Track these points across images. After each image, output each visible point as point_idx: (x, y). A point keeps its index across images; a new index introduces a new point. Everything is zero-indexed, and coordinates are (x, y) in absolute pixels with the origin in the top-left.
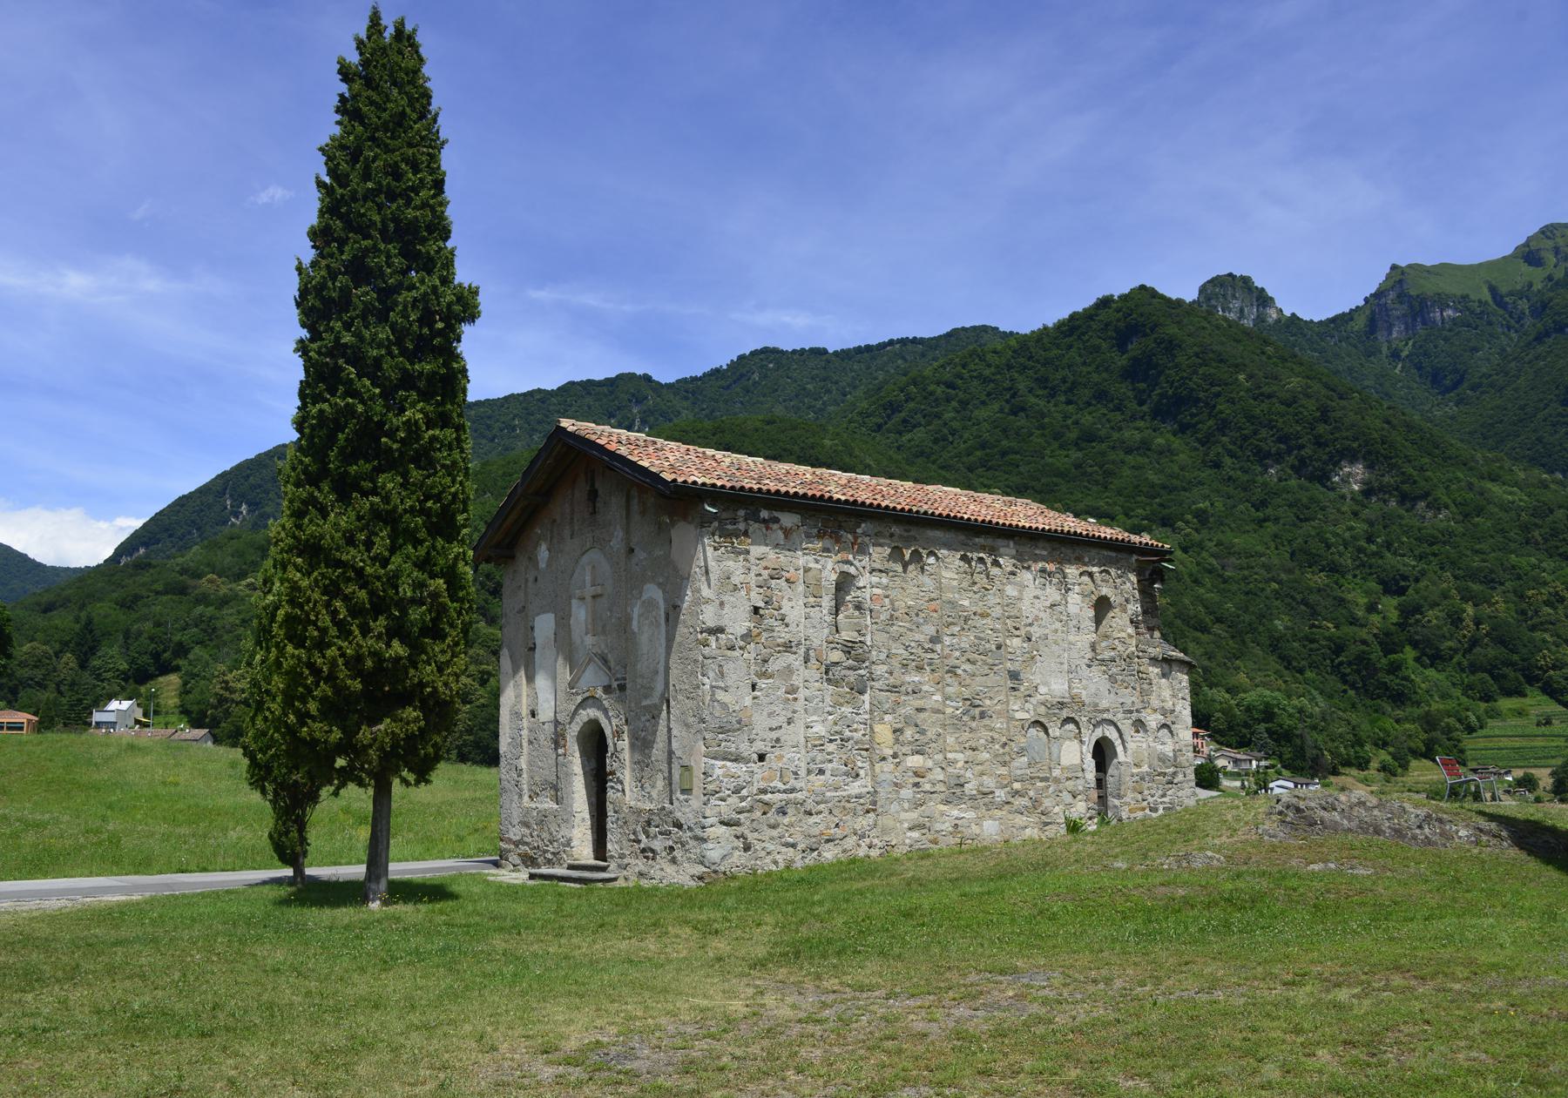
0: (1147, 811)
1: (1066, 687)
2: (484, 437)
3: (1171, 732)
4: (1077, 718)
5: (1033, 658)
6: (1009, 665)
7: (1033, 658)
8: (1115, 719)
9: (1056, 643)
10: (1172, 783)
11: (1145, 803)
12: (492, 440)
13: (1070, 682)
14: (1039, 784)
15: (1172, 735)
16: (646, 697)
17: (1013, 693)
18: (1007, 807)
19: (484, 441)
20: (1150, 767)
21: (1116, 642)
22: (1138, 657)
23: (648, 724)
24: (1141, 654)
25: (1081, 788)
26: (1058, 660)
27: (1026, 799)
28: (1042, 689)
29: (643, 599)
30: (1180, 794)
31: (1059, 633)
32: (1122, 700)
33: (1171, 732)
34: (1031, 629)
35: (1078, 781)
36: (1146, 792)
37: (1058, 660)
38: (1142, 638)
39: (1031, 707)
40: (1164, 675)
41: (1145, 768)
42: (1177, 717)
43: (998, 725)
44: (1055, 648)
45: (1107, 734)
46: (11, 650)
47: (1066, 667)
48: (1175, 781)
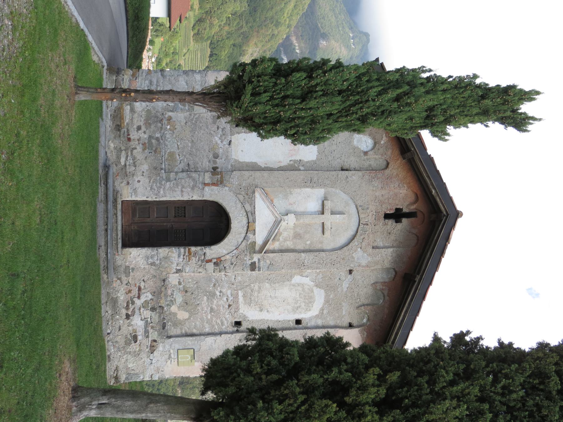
16: (244, 296)
23: (225, 299)
29: (315, 288)
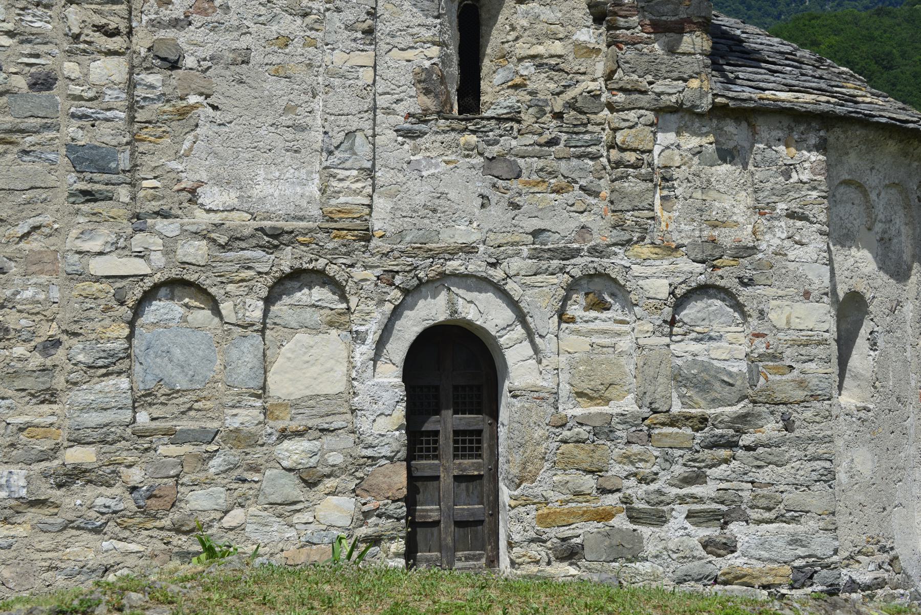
0: (620, 522)
1: (313, 189)
2: (769, 15)
3: (739, 307)
4: (332, 270)
5: (183, 114)
6: (72, 130)
7: (183, 114)
8: (497, 274)
9: (281, 73)
10: (731, 445)
11: (611, 500)
12: (778, 17)
13: (328, 173)
14: (167, 450)
15: (745, 315)
17: (85, 208)
18: (33, 514)
19: (769, 20)
20: (639, 400)
21: (527, 69)
22: (611, 107)
24: (620, 97)
25: (336, 459)
26: (286, 120)
27: (117, 490)
28: (211, 197)
30: (763, 476)
31: (296, 47)
32: (537, 224)
33: (739, 307)
34: (182, 38)
35: (328, 439)
36: (617, 469)
37: (286, 120)
38: (629, 54)
39: (155, 243)
40: (726, 155)
41: (627, 404)
42: (758, 267)
43: (28, 294)
44: (274, 86)
45: (469, 313)
46: (128, 325)
47: (316, 137)
48: (746, 440)
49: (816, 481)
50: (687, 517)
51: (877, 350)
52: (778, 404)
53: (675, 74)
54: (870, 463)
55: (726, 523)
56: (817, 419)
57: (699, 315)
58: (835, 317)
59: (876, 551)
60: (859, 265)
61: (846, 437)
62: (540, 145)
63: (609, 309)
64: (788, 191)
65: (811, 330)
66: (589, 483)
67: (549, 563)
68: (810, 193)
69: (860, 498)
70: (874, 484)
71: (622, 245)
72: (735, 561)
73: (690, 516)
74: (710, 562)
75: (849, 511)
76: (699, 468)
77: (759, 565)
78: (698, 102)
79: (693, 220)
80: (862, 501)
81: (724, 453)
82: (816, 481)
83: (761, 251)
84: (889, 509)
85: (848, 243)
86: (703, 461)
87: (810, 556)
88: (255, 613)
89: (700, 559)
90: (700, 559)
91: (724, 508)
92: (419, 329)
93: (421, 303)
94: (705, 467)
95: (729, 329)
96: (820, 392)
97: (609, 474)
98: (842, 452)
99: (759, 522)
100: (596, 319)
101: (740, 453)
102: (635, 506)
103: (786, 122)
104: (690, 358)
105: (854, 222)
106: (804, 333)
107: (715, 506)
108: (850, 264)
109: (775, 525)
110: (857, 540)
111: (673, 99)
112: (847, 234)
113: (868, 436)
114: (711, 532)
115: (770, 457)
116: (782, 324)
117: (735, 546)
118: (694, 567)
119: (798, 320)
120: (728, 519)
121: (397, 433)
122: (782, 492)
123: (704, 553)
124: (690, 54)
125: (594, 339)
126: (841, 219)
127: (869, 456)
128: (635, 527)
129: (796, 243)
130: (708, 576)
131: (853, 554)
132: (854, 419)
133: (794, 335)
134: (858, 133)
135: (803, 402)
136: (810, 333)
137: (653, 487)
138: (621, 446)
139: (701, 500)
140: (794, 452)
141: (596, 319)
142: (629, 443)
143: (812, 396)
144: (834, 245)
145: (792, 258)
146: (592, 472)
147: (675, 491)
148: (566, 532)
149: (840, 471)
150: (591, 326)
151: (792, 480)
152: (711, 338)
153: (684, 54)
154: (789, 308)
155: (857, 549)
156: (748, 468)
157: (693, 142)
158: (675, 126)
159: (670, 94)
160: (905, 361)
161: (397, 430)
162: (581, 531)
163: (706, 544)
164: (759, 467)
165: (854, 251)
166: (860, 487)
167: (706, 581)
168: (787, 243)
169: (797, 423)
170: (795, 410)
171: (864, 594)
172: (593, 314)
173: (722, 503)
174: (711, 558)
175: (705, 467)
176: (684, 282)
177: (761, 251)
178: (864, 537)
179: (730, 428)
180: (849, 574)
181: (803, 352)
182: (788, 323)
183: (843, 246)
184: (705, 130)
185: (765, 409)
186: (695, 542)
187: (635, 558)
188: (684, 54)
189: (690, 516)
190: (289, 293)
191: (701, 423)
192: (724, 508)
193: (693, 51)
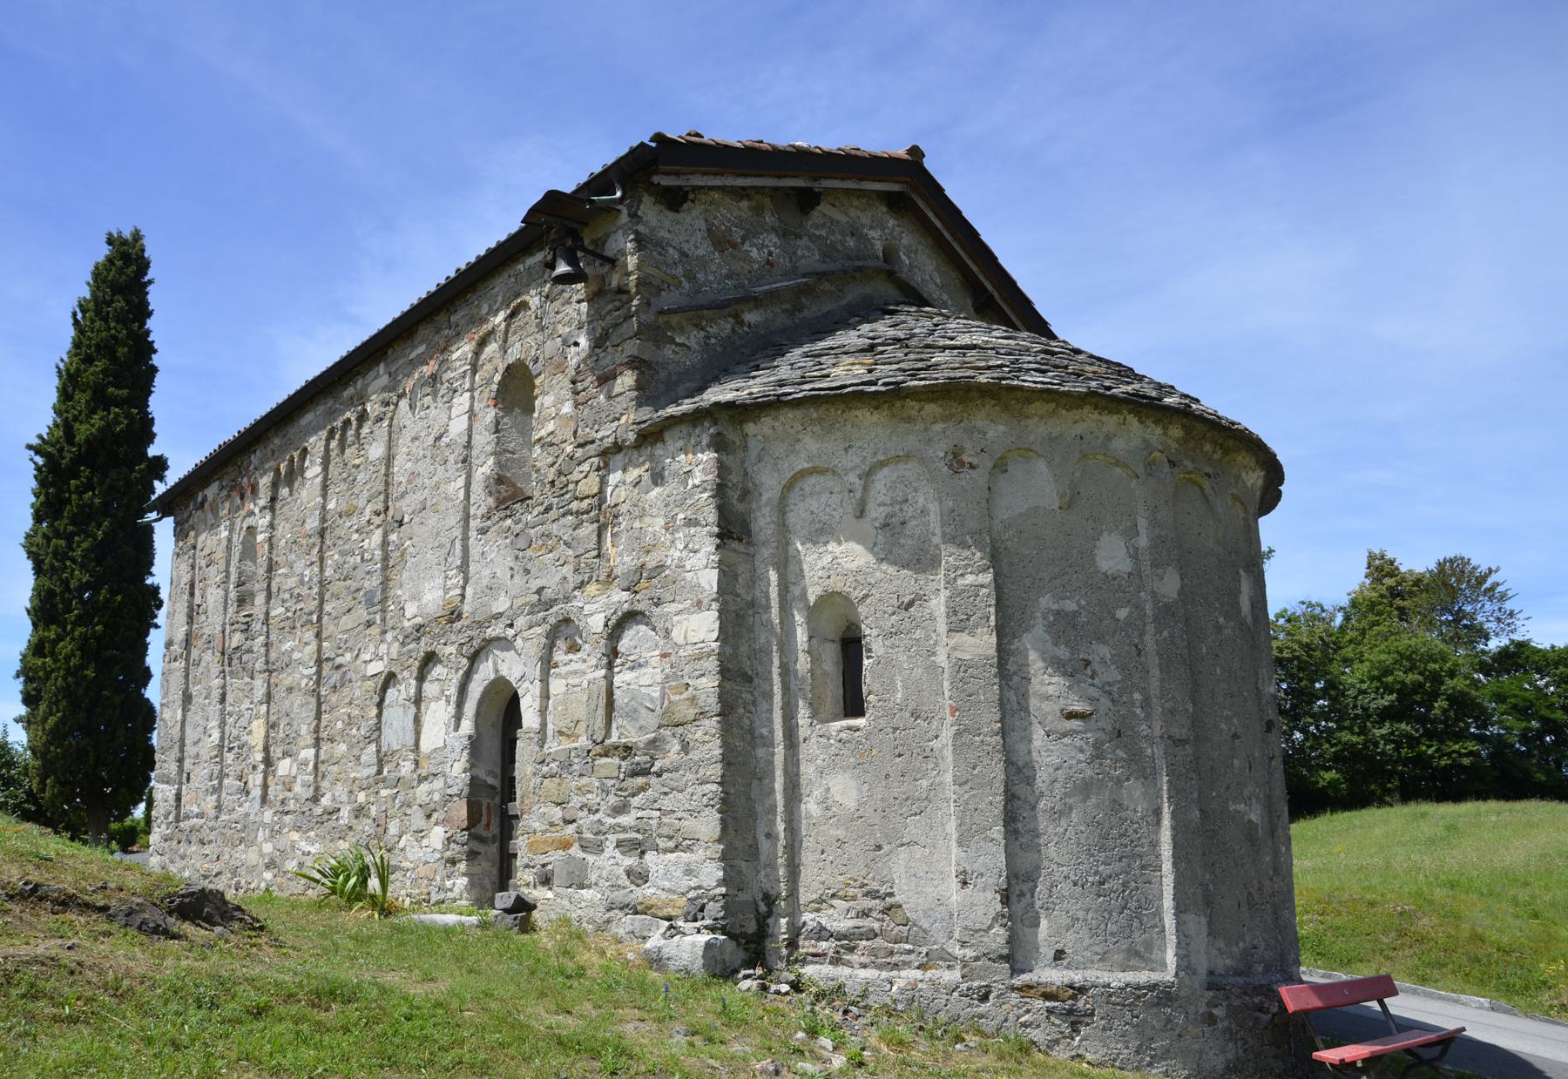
0: (575, 851)
36: (576, 801)
49: (706, 806)
50: (617, 846)
51: (872, 657)
52: (678, 726)
53: (611, 418)
54: (855, 792)
55: (643, 853)
56: (707, 738)
57: (631, 643)
58: (804, 625)
59: (860, 895)
60: (840, 560)
61: (819, 762)
62: (543, 514)
63: (579, 650)
64: (686, 499)
65: (703, 642)
66: (557, 813)
67: (535, 887)
68: (702, 495)
69: (840, 833)
70: (861, 817)
71: (580, 588)
72: (647, 892)
73: (619, 845)
74: (632, 891)
75: (820, 847)
76: (625, 797)
77: (664, 896)
78: (625, 436)
79: (634, 550)
80: (841, 837)
81: (640, 780)
82: (706, 806)
83: (668, 567)
84: (886, 848)
85: (823, 539)
86: (626, 790)
87: (700, 887)
88: (1489, 1078)
89: (624, 888)
90: (624, 888)
91: (640, 837)
92: (481, 689)
93: (481, 667)
94: (628, 796)
95: (651, 654)
96: (707, 709)
97: (570, 805)
98: (814, 779)
99: (666, 851)
100: (571, 661)
101: (653, 780)
102: (584, 836)
103: (685, 428)
104: (625, 687)
105: (834, 513)
106: (697, 646)
107: (634, 835)
108: (825, 562)
109: (675, 855)
110: (830, 881)
111: (611, 440)
112: (823, 528)
113: (852, 760)
114: (630, 861)
115: (672, 782)
116: (680, 641)
117: (648, 876)
118: (619, 896)
119: (693, 633)
120: (643, 848)
121: (464, 775)
122: (680, 819)
123: (628, 883)
124: (621, 394)
125: (571, 681)
126: (812, 513)
127: (853, 783)
128: (585, 856)
129: (691, 551)
130: (628, 905)
131: (824, 897)
132: (832, 741)
133: (690, 650)
134: (790, 415)
135: (694, 720)
136: (702, 645)
137: (597, 816)
138: (576, 778)
139: (624, 830)
140: (690, 776)
141: (571, 661)
142: (581, 775)
143: (702, 713)
144: (802, 544)
145: (688, 568)
146: (558, 804)
147: (610, 821)
148: (544, 859)
149: (809, 802)
150: (568, 668)
151: (687, 806)
152: (640, 666)
153: (617, 396)
154: (685, 622)
155: (831, 892)
156: (657, 795)
157: (634, 473)
158: (620, 464)
159: (608, 437)
160: (934, 666)
161: (464, 772)
162: (552, 859)
163: (629, 873)
164: (665, 794)
165: (832, 546)
166: (839, 820)
167: (627, 911)
168: (685, 554)
169: (691, 744)
170: (689, 731)
171: (838, 943)
172: (571, 656)
173: (638, 831)
174: (633, 887)
175: (628, 796)
176: (615, 613)
177: (668, 567)
178: (841, 878)
179: (646, 754)
180: (818, 919)
181: (698, 667)
182: (685, 638)
183: (815, 543)
184: (641, 460)
185: (669, 733)
186: (621, 871)
187: (582, 887)
188: (617, 396)
189: (619, 845)
190: (429, 672)
191: (625, 751)
192: (640, 837)
193: (623, 390)
